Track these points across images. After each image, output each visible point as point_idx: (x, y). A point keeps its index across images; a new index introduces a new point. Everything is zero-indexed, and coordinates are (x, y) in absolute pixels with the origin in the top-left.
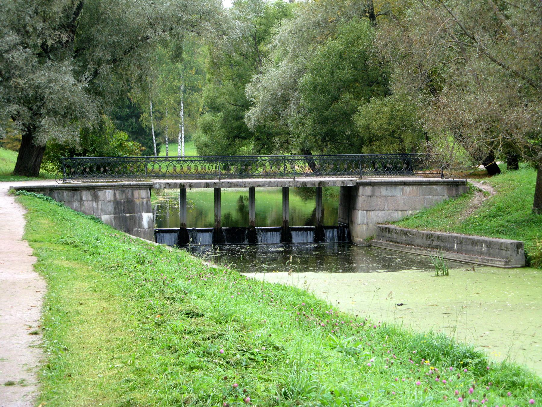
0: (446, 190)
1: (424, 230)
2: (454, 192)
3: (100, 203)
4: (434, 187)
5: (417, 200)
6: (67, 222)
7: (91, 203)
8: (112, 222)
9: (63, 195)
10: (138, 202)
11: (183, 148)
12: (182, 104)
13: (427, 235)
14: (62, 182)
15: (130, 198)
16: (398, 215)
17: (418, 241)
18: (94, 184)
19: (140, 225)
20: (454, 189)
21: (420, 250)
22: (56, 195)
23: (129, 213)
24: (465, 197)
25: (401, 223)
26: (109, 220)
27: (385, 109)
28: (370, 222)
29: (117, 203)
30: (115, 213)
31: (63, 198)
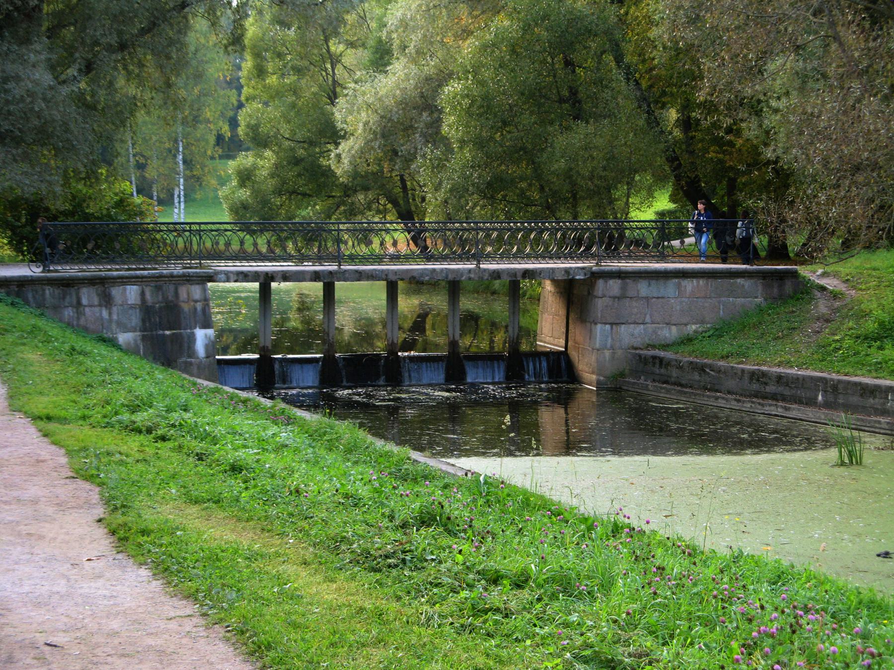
0: (760, 288)
1: (742, 363)
2: (776, 290)
3: (115, 309)
4: (739, 280)
5: (706, 305)
6: (81, 358)
7: (97, 309)
8: (137, 346)
9: (43, 294)
10: (186, 307)
11: (182, 211)
12: (181, 143)
13: (753, 374)
14: (41, 269)
15: (172, 301)
16: (670, 333)
17: (731, 384)
18: (103, 274)
19: (192, 353)
20: (776, 285)
21: (738, 401)
22: (30, 295)
23: (169, 329)
24: (798, 299)
25: (681, 348)
26: (132, 342)
27: (599, 141)
28: (618, 344)
29: (146, 310)
30: (143, 329)
31: (44, 299)
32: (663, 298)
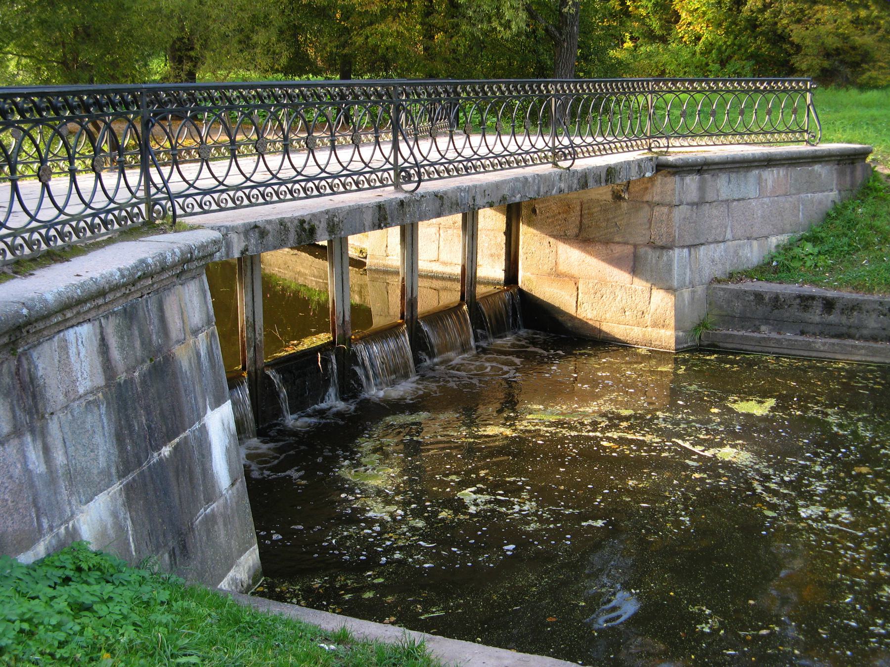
3: (53, 427)
26: (109, 521)
32: (743, 199)
